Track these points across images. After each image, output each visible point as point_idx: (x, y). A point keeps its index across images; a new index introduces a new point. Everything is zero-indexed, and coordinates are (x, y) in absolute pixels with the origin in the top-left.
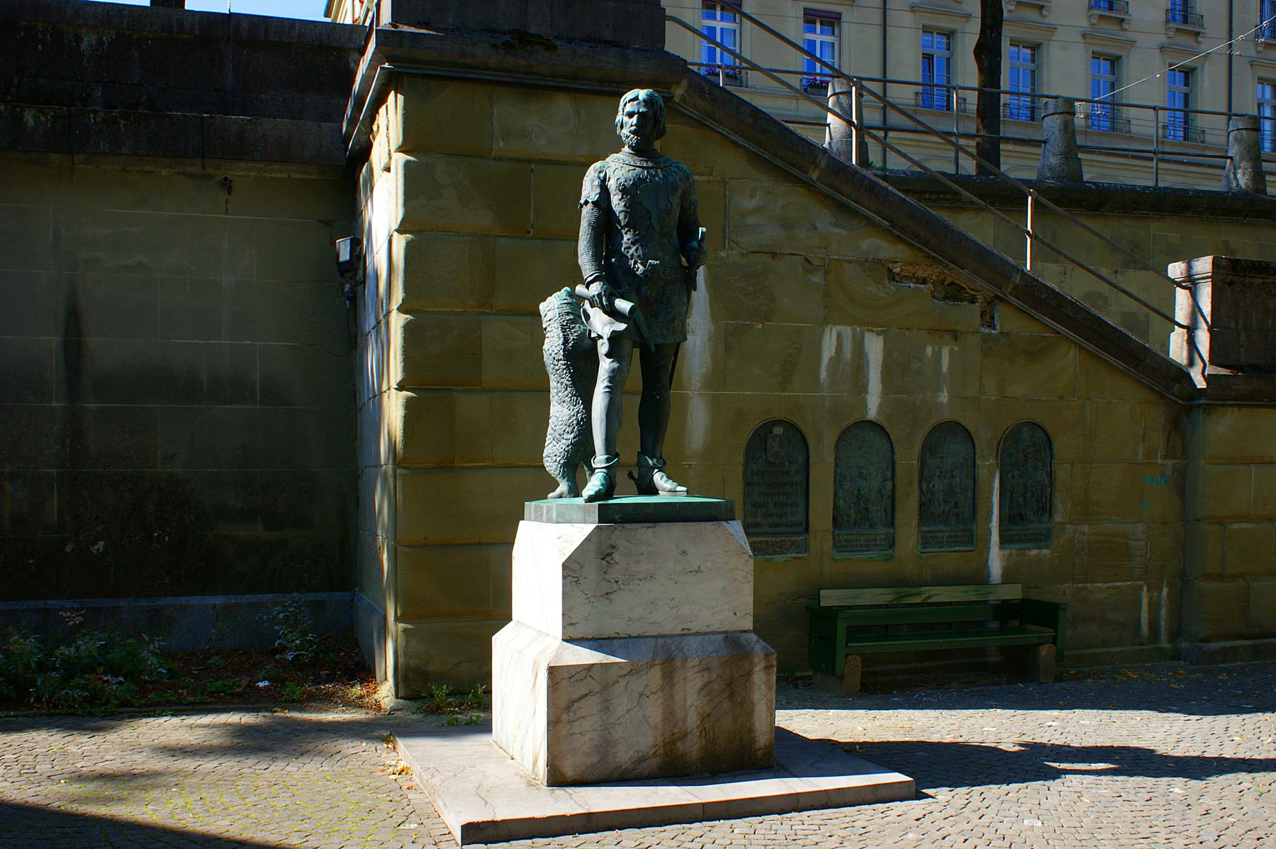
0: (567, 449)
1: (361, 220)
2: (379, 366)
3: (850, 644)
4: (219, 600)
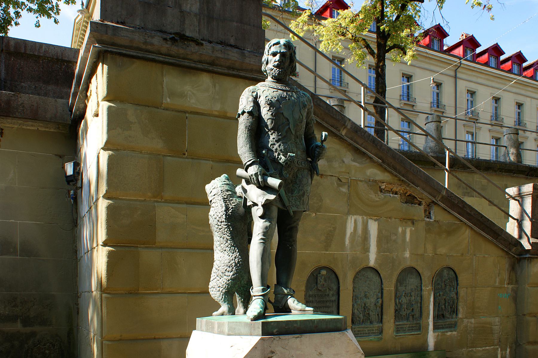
1: (80, 154)
2: (91, 236)
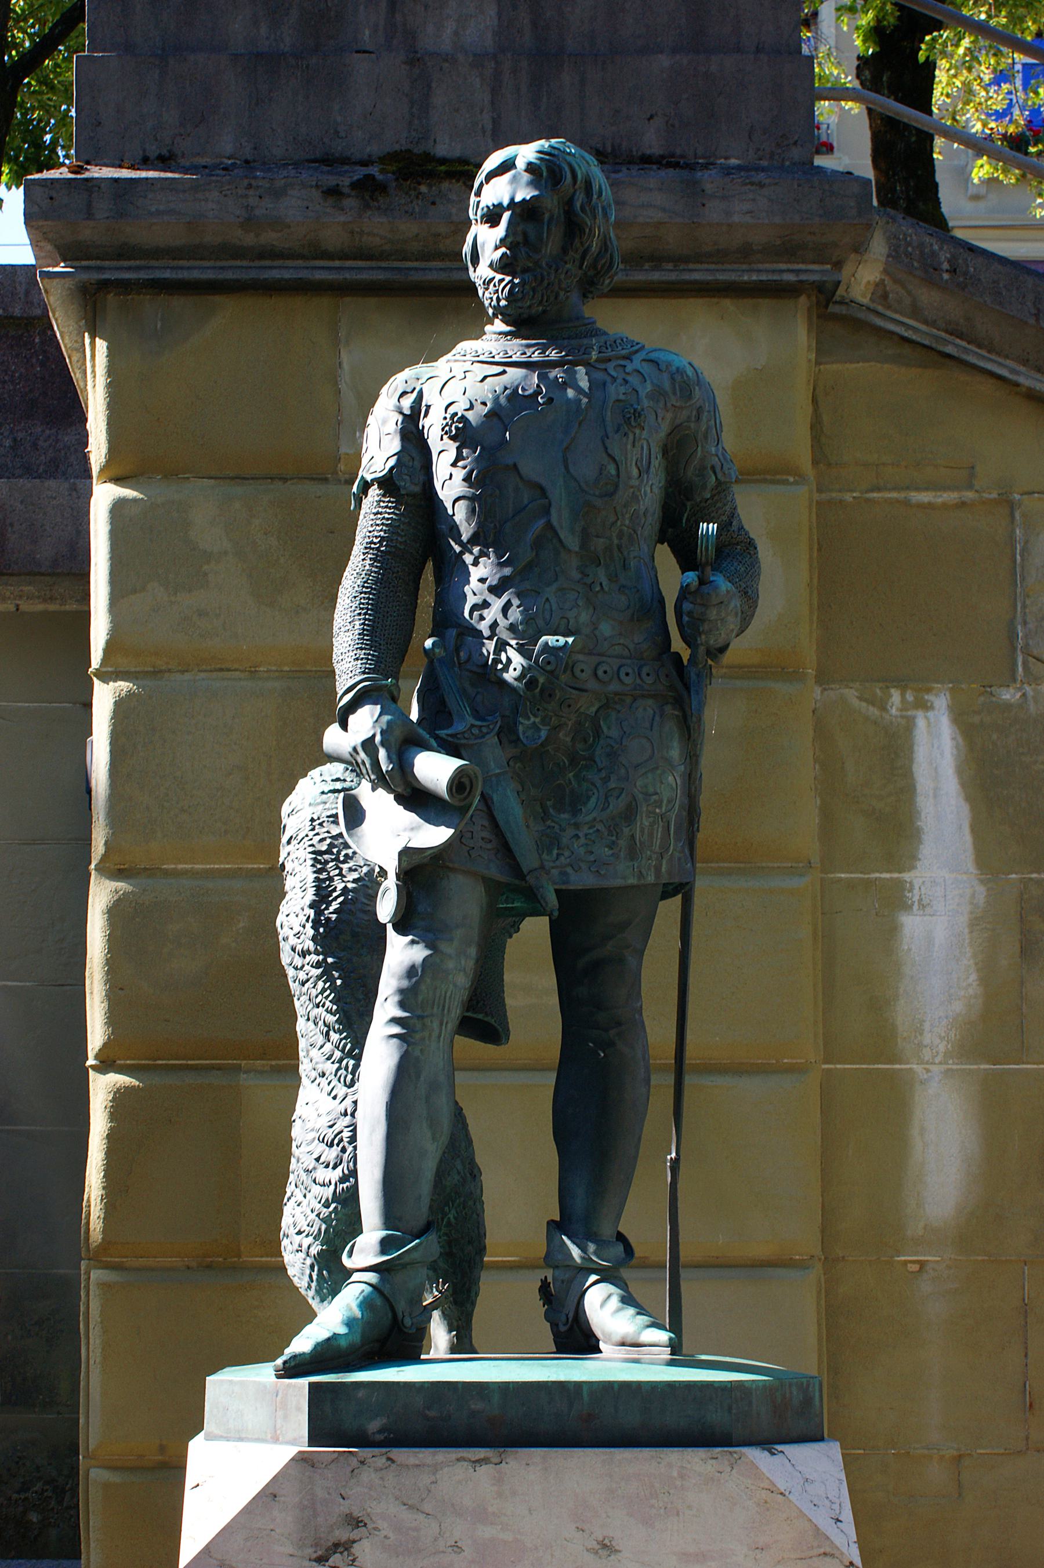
0: (325, 1212)
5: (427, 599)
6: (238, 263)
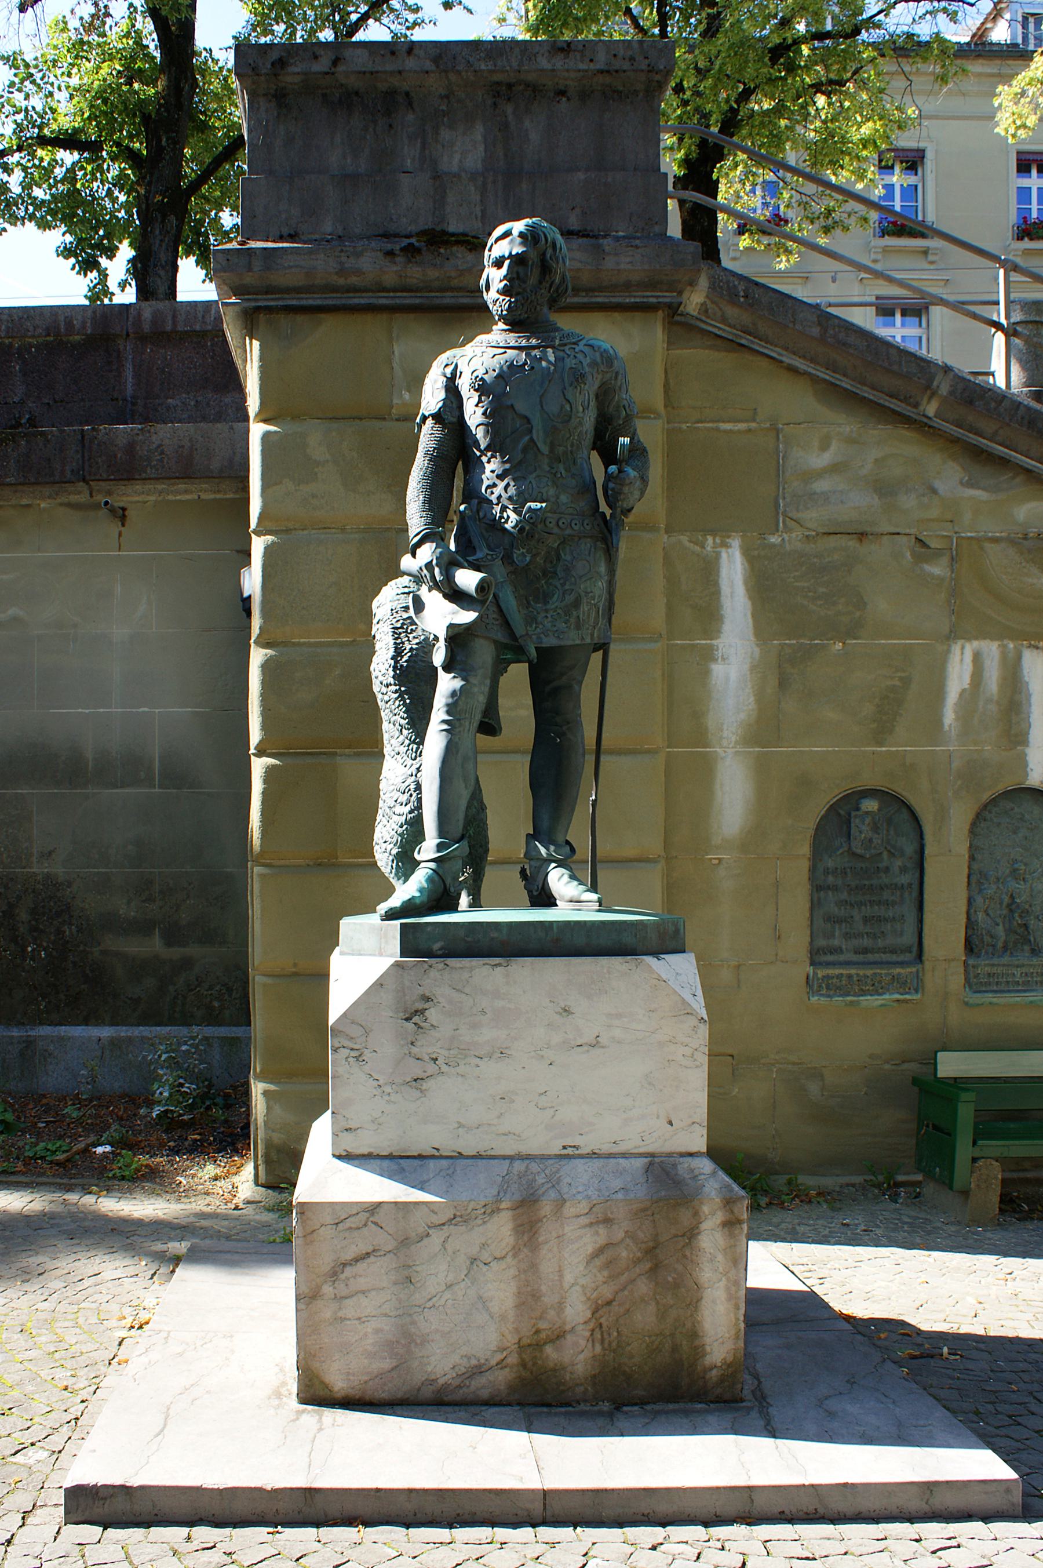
0: (400, 830)
3: (980, 1142)
4: (106, 1032)
5: (459, 483)
6: (335, 295)
